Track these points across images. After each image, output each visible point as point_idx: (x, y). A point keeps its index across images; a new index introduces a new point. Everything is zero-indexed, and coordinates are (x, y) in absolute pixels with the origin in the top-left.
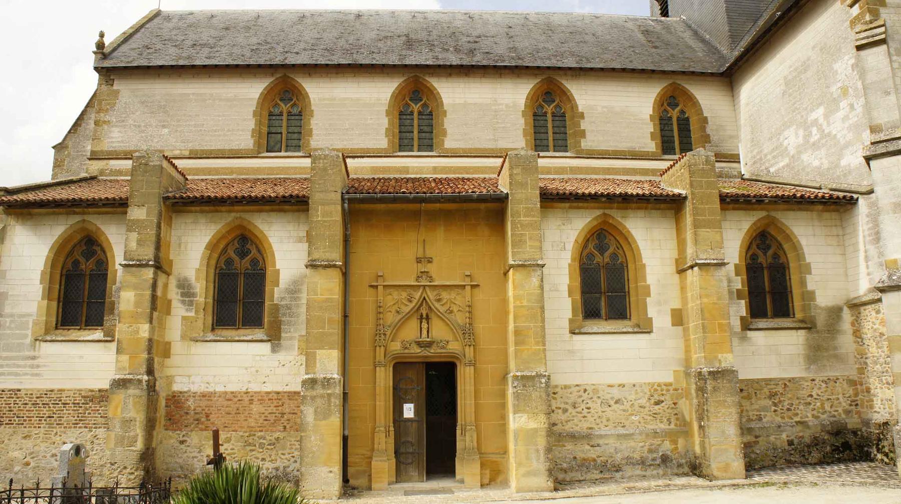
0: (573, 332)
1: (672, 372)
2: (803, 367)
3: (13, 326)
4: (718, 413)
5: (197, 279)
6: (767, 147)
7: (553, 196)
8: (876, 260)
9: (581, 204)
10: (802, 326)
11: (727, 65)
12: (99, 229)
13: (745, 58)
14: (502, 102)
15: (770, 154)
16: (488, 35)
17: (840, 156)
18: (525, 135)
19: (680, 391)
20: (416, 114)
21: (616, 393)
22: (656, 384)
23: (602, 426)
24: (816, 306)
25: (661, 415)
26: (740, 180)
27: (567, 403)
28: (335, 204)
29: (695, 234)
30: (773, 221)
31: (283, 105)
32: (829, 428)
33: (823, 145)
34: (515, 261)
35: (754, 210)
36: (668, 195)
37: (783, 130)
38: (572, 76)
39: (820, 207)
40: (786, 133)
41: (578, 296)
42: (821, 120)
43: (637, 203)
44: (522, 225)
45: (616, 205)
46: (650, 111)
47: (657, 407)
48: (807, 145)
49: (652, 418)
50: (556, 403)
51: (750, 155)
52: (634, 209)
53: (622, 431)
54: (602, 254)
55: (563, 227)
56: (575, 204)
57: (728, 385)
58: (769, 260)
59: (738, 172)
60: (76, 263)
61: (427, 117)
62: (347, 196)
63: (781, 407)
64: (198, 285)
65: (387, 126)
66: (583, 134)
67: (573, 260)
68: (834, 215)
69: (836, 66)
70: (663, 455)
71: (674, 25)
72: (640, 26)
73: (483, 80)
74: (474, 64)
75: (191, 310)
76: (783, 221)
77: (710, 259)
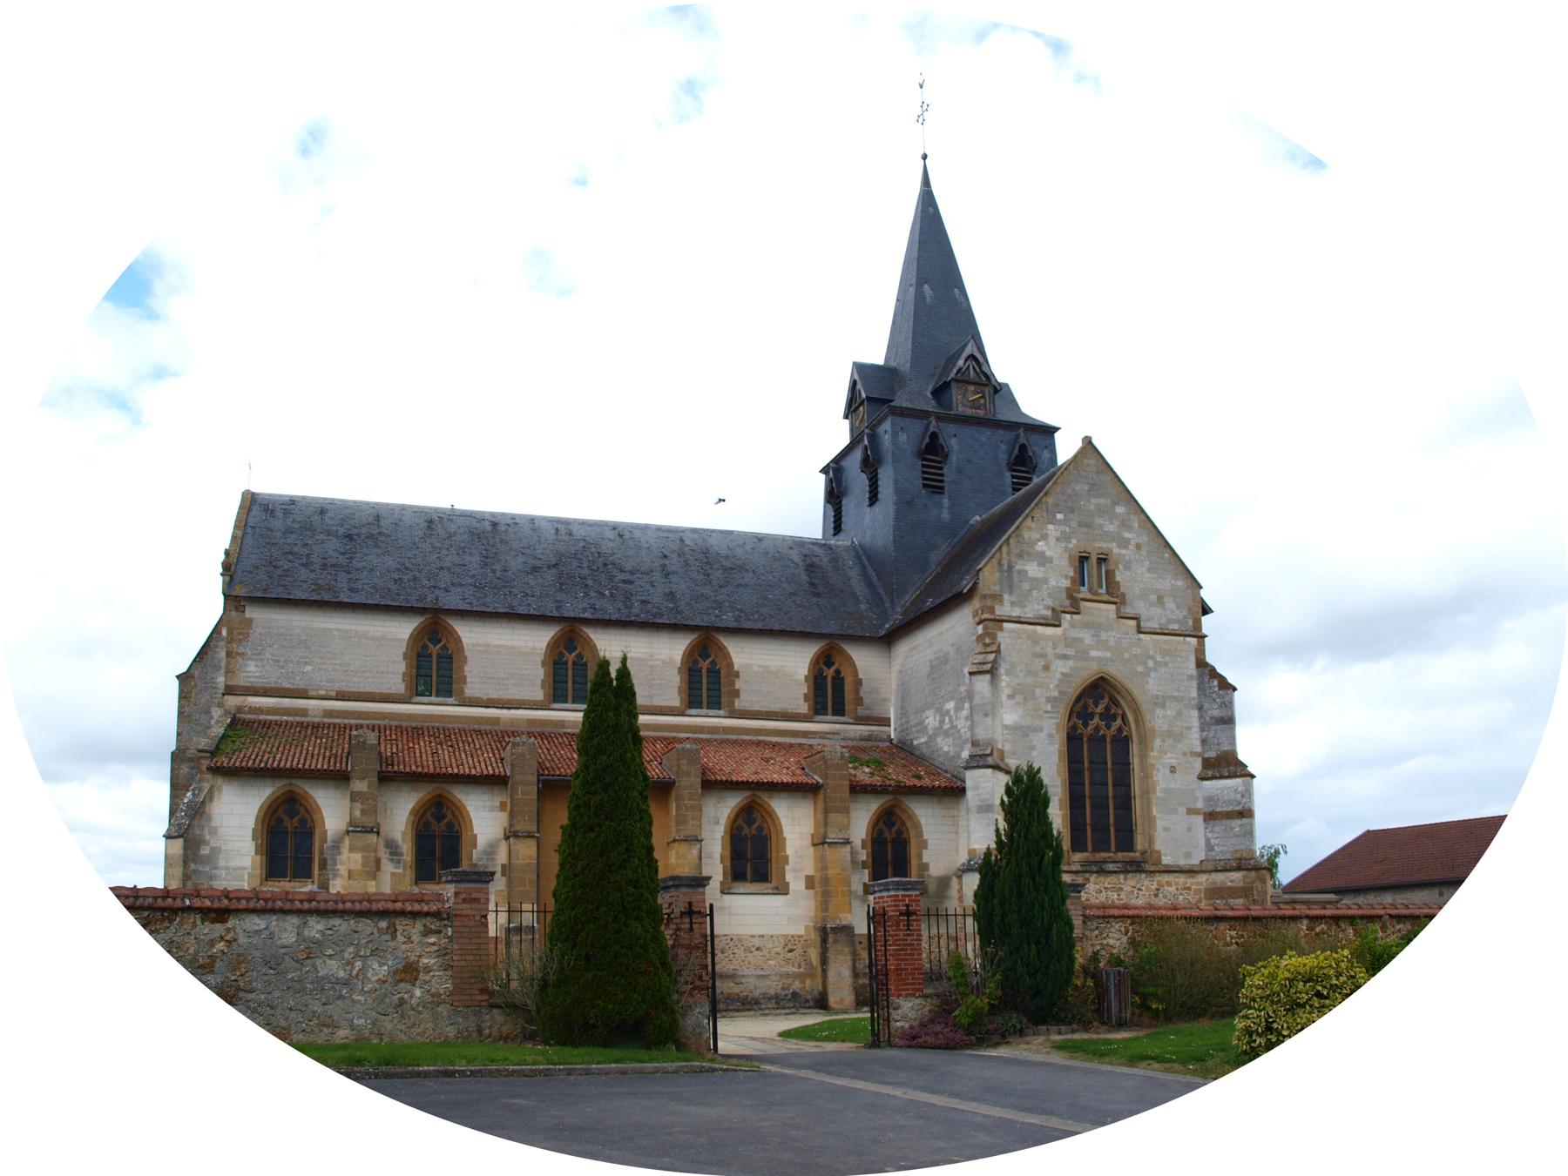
0: (723, 892)
3: (229, 877)
5: (403, 840)
6: (913, 720)
11: (887, 626)
12: (307, 792)
14: (658, 657)
18: (680, 692)
19: (809, 942)
20: (570, 663)
21: (757, 942)
24: (929, 875)
28: (532, 785)
31: (432, 646)
33: (952, 735)
41: (728, 864)
42: (952, 713)
46: (805, 671)
47: (790, 954)
48: (939, 730)
51: (899, 722)
53: (761, 973)
55: (718, 805)
60: (280, 821)
61: (582, 667)
62: (541, 778)
64: (405, 846)
65: (543, 677)
66: (736, 694)
67: (725, 832)
70: (793, 992)
72: (805, 556)
73: (641, 633)
75: (399, 868)
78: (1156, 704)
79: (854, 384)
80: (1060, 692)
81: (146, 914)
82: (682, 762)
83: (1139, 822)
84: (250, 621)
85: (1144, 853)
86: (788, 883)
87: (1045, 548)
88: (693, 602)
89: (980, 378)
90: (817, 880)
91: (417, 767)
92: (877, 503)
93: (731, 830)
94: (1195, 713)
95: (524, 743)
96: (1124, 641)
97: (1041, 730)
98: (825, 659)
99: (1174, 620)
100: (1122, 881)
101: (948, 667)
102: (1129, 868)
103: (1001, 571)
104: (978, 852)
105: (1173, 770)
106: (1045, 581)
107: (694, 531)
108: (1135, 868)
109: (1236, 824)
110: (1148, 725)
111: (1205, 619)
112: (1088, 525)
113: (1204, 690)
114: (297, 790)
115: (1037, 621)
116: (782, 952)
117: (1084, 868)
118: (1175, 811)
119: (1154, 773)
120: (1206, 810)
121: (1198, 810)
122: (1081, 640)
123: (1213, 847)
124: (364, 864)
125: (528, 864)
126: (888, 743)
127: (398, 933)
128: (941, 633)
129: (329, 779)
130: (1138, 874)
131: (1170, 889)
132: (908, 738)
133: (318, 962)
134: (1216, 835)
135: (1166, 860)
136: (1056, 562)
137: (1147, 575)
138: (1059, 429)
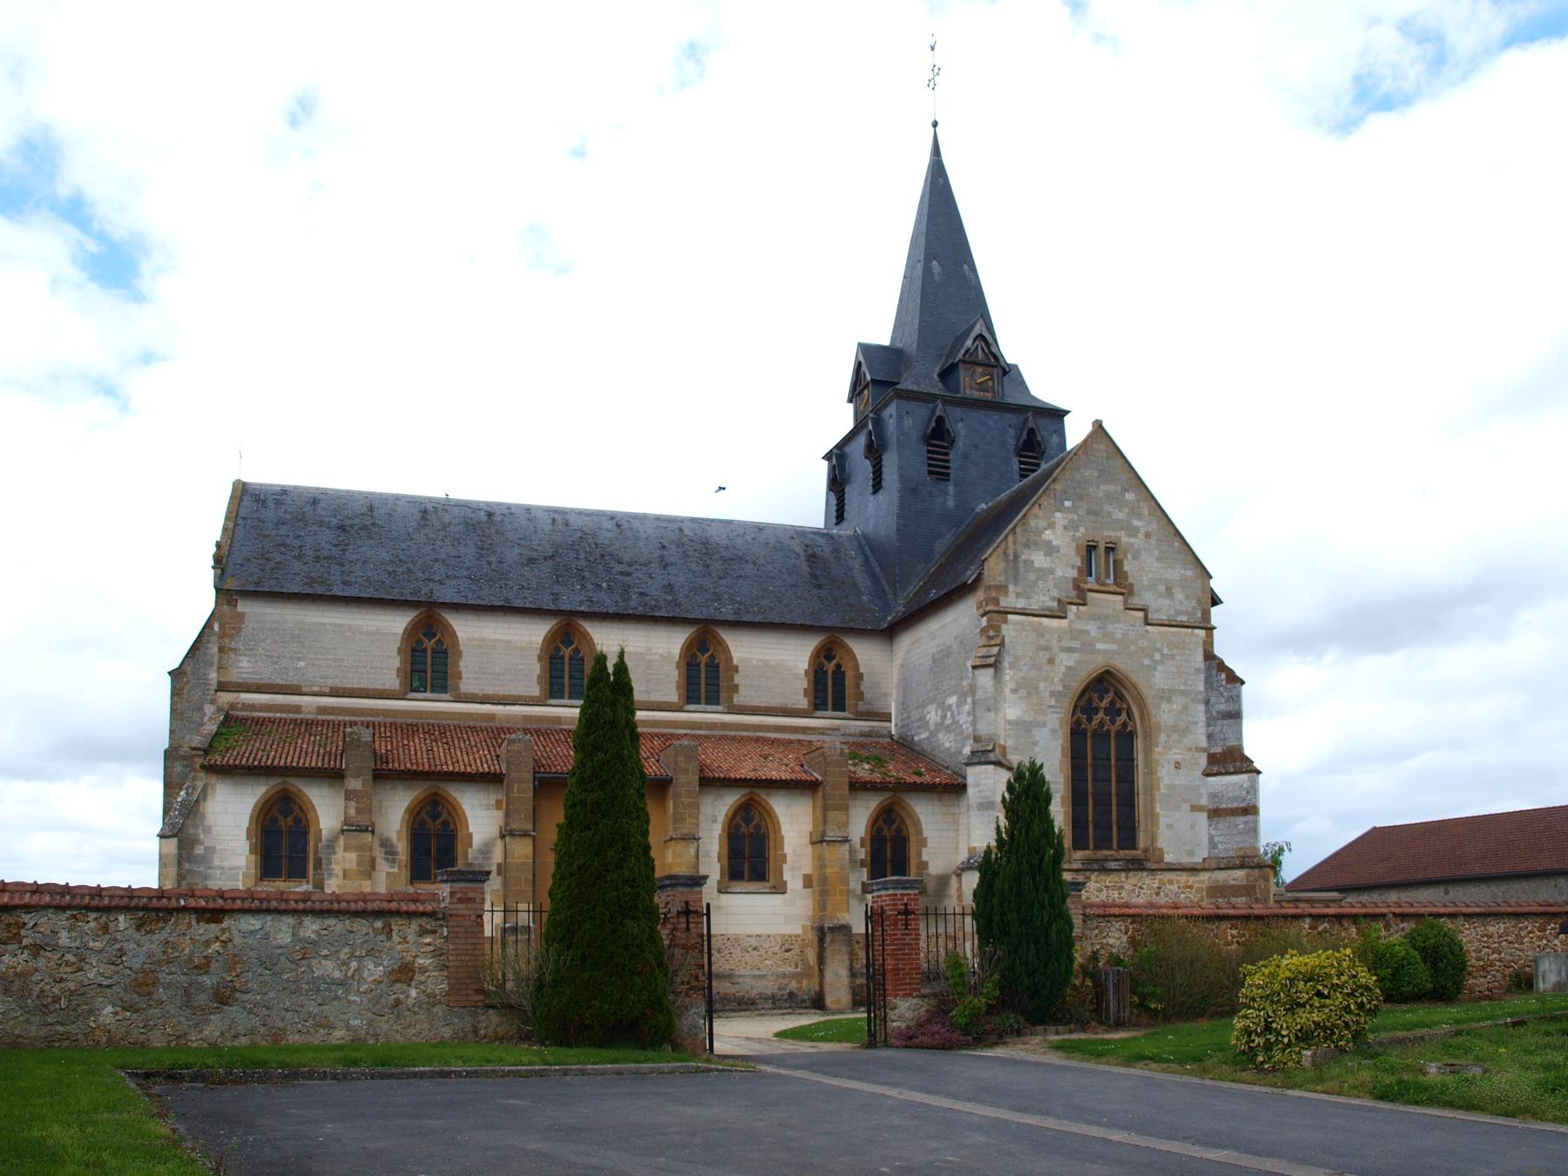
0: (720, 891)
5: (399, 839)
6: (915, 715)
11: (889, 618)
18: (678, 688)
20: (567, 658)
21: (754, 942)
23: (741, 968)
40: (929, 708)
41: (725, 862)
42: (954, 707)
46: (805, 666)
48: (941, 726)
53: (758, 973)
58: (893, 833)
60: (274, 820)
62: (537, 775)
66: (735, 688)
67: (723, 830)
73: (638, 626)
75: (394, 867)
78: (1162, 698)
79: (858, 366)
80: (1064, 686)
81: (141, 914)
84: (242, 615)
85: (1146, 850)
86: (786, 883)
87: (1052, 537)
89: (989, 359)
90: (815, 878)
91: (412, 765)
92: (881, 491)
93: (729, 827)
94: (1202, 708)
95: (520, 740)
96: (1131, 633)
97: (1044, 725)
98: (825, 653)
100: (1123, 879)
101: (950, 661)
102: (1131, 867)
105: (1177, 766)
106: (1051, 571)
107: (693, 520)
108: (1136, 866)
109: (1241, 820)
110: (1154, 720)
111: (1213, 610)
112: (1096, 513)
114: (292, 789)
115: (1043, 613)
117: (1086, 866)
118: (1178, 808)
119: (1159, 768)
120: (1211, 807)
122: (1087, 632)
124: (359, 864)
125: (524, 863)
126: (889, 740)
127: (394, 934)
128: (944, 626)
129: (323, 777)
130: (1140, 873)
131: (1171, 887)
132: (909, 734)
133: (314, 962)
134: (1220, 833)
135: (1169, 858)
136: (1063, 551)
137: (1156, 565)
138: (1068, 412)
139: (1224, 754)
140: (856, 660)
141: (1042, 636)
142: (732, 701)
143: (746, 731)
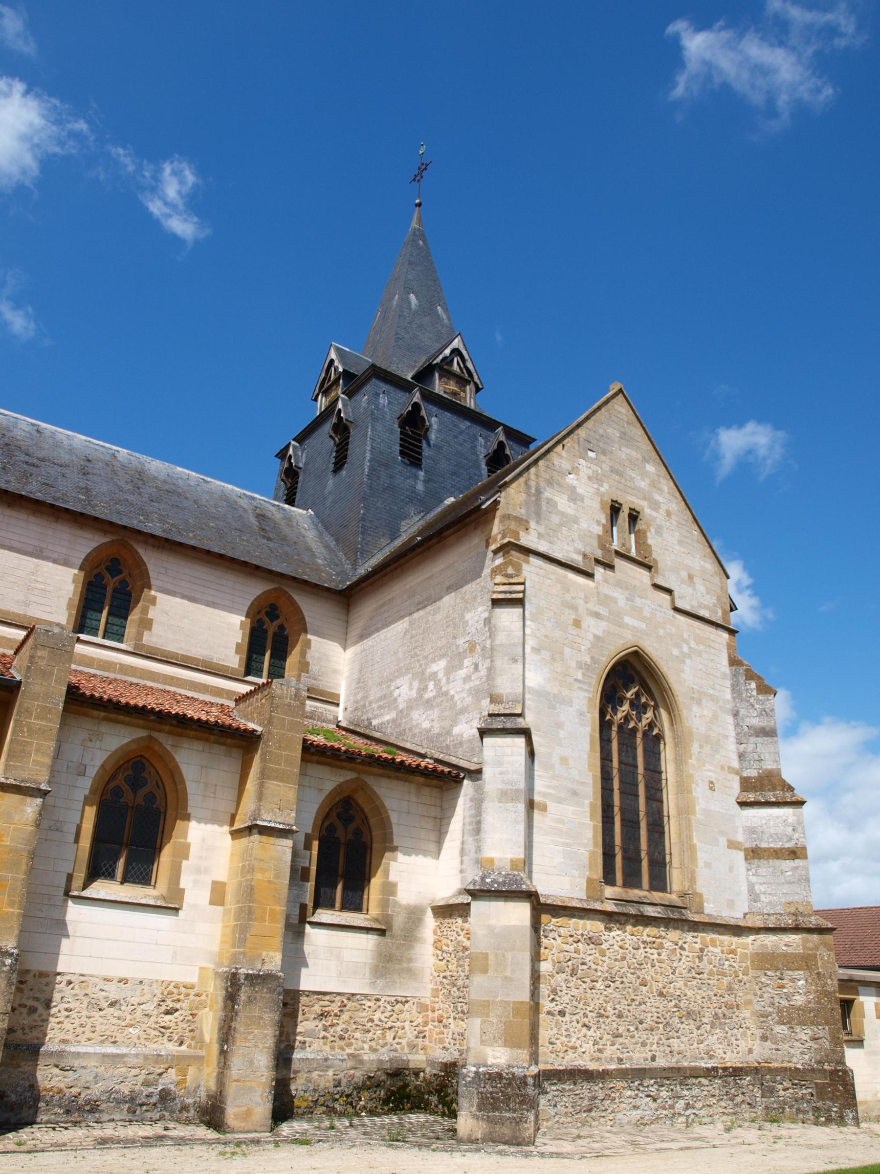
1: (197, 969)
2: (367, 980)
4: (249, 1033)
6: (375, 693)
7: (225, 728)
8: (473, 854)
9: (121, 718)
10: (374, 927)
11: (348, 583)
13: (370, 580)
15: (376, 702)
16: (56, 461)
17: (455, 722)
18: (69, 607)
19: (203, 997)
21: (114, 992)
22: (172, 984)
24: (396, 902)
25: (171, 1030)
26: (334, 726)
27: (37, 999)
29: (261, 786)
30: (363, 787)
32: (388, 1065)
33: (439, 705)
34: (7, 778)
35: (343, 768)
36: (238, 729)
37: (396, 677)
38: (153, 546)
39: (421, 779)
40: (399, 682)
42: (441, 675)
43: (196, 730)
44: (30, 730)
45: (167, 728)
48: (420, 701)
49: (158, 1033)
50: (22, 998)
52: (192, 738)
54: (135, 790)
55: (89, 744)
56: (113, 716)
57: (268, 995)
59: (334, 716)
63: (331, 1033)
68: (435, 793)
69: (468, 616)
71: (298, 517)
72: (256, 507)
73: (32, 519)
74: (23, 493)
76: (375, 788)
77: (275, 822)
80: (592, 658)
82: (39, 654)
83: (675, 851)
85: (683, 895)
86: (183, 891)
87: (575, 483)
88: (112, 503)
89: (463, 372)
94: (730, 719)
96: (659, 614)
97: (570, 703)
99: (705, 605)
103: (528, 495)
104: (496, 863)
106: (576, 520)
112: (620, 474)
113: (740, 694)
116: (156, 1012)
119: (694, 786)
121: (739, 843)
122: (615, 601)
123: (757, 895)
132: (365, 717)
134: (762, 880)
136: (587, 501)
137: (677, 547)
139: (760, 778)
140: (305, 624)
141: (568, 590)
142: (141, 639)
143: (153, 681)
